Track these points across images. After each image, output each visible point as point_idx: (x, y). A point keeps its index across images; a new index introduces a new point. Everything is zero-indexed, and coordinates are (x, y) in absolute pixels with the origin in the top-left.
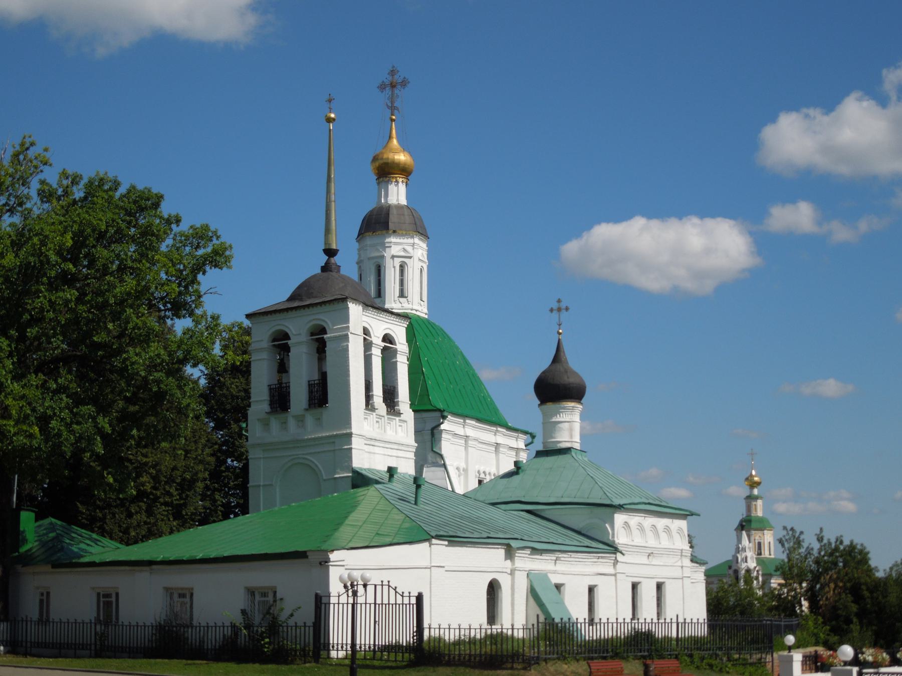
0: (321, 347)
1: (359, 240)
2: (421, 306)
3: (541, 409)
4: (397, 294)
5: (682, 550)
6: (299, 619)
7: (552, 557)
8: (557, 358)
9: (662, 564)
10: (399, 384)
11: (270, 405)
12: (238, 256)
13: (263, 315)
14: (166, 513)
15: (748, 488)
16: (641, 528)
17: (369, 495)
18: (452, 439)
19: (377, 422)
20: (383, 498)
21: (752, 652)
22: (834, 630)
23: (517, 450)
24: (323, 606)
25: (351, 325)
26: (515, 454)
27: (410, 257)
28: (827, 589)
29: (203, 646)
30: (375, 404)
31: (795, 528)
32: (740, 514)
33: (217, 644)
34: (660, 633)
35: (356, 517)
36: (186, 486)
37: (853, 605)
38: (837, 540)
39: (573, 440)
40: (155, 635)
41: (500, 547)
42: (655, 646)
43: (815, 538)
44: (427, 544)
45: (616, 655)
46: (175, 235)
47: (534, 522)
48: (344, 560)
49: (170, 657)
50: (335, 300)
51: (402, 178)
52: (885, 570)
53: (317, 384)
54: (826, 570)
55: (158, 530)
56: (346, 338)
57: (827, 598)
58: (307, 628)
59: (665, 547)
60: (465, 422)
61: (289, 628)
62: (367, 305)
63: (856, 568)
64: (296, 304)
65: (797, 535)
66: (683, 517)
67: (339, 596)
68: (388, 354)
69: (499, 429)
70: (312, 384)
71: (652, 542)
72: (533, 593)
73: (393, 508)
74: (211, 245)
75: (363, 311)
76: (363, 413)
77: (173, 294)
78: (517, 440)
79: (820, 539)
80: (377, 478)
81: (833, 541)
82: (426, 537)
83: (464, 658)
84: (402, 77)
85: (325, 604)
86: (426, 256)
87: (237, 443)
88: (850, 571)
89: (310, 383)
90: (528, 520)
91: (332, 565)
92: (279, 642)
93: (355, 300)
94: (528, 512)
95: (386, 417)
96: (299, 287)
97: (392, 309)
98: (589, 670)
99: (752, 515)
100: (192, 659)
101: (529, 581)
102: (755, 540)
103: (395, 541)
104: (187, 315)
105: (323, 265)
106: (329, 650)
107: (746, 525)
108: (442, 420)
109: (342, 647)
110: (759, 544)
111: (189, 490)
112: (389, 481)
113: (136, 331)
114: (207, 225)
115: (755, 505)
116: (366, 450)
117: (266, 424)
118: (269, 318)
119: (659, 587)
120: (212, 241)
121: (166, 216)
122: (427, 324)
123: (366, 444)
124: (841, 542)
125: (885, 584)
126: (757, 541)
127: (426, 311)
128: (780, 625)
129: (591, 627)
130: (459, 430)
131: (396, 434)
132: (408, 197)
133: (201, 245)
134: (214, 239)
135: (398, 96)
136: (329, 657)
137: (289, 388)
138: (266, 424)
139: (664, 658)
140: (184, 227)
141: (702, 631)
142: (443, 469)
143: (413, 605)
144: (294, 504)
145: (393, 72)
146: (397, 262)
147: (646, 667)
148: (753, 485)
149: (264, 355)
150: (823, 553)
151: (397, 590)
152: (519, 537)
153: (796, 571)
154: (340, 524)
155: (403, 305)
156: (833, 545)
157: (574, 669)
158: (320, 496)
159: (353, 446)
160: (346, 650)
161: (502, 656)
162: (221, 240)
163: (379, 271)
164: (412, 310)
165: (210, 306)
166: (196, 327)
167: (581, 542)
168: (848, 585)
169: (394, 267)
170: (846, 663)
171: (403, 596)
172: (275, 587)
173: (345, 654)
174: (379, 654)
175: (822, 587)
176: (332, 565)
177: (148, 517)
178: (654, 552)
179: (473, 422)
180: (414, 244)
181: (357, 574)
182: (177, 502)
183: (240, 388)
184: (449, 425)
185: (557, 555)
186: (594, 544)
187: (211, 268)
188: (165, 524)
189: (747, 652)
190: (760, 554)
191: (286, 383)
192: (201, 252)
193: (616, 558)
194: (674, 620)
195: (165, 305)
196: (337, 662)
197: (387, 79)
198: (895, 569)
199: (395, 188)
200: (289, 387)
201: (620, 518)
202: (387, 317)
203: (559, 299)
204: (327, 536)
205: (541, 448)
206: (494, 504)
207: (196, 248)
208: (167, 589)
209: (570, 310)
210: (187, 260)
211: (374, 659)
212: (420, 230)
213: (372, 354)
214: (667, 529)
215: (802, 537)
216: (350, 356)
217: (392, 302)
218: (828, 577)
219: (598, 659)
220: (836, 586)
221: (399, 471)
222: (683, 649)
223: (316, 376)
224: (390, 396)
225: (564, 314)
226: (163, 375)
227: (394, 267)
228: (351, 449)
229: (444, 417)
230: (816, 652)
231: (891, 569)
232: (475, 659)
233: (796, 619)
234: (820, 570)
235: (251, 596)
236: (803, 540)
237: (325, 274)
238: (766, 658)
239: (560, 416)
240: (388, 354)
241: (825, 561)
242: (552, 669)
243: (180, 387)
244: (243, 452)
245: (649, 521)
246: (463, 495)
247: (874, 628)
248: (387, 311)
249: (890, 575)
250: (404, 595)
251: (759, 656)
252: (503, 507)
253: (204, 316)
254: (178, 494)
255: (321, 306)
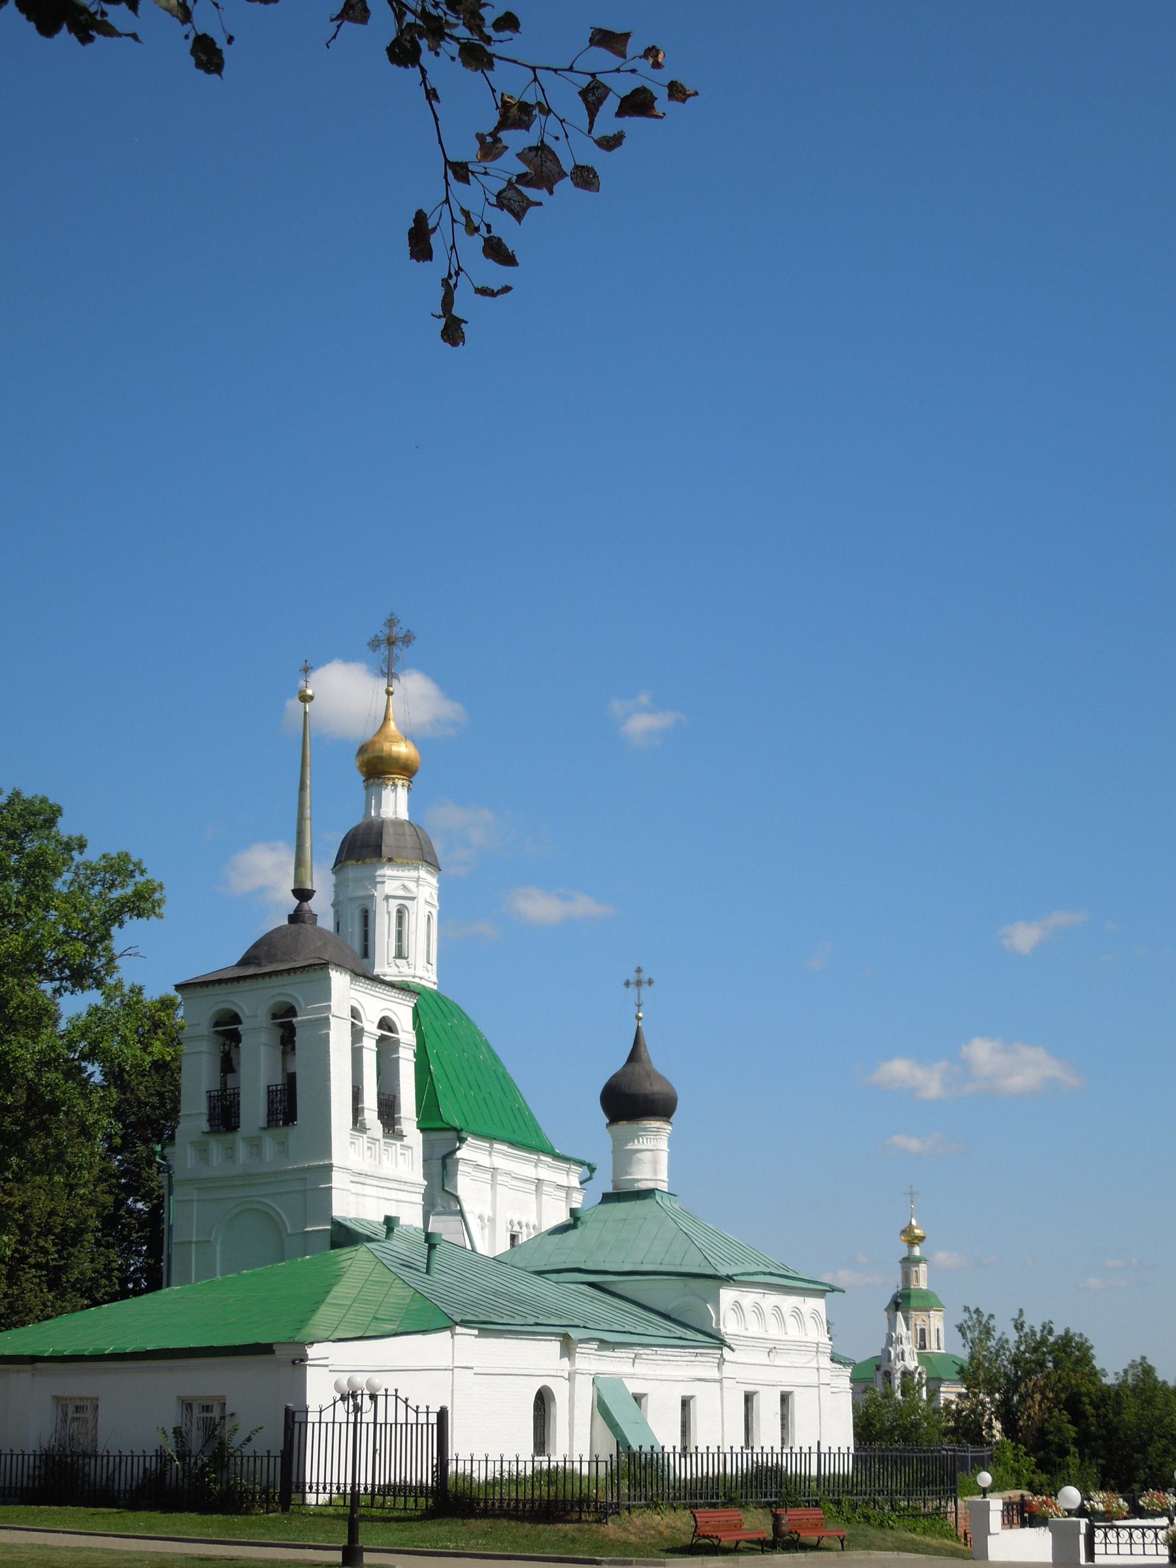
0: (287, 1036)
1: (339, 869)
2: (428, 971)
3: (611, 1132)
4: (393, 953)
5: (817, 1344)
6: (260, 1445)
7: (629, 1353)
8: (635, 1055)
9: (788, 1364)
10: (401, 1091)
11: (209, 1120)
12: (172, 900)
13: (201, 987)
14: (38, 1280)
15: (905, 1245)
16: (758, 1310)
17: (356, 1258)
18: (473, 1173)
19: (369, 1148)
20: (380, 1264)
21: (927, 1497)
22: (1043, 1465)
23: (569, 1189)
24: (297, 1425)
25: (334, 1003)
26: (564, 1195)
27: (413, 899)
28: (1029, 1402)
29: (113, 1486)
30: (367, 1122)
31: (981, 1310)
32: (893, 1285)
33: (135, 1483)
34: (792, 1467)
35: (342, 1292)
36: (69, 1238)
37: (1070, 1426)
38: (1044, 1327)
39: (659, 1178)
40: (40, 1467)
41: (553, 1338)
42: (786, 1488)
43: (1013, 1323)
44: (448, 1333)
45: (730, 1502)
46: (77, 867)
47: (598, 1300)
48: (328, 1358)
49: (60, 1503)
50: (311, 965)
51: (404, 779)
52: (1116, 1374)
53: (280, 1090)
54: (1029, 1373)
55: (24, 1306)
56: (326, 1022)
57: (1029, 1416)
58: (272, 1459)
59: (794, 1339)
60: (491, 1147)
61: (245, 1460)
62: (357, 975)
63: (1073, 1371)
64: (251, 971)
65: (984, 1320)
66: (821, 1294)
67: (321, 1412)
68: (387, 1047)
69: (542, 1158)
70: (273, 1091)
71: (774, 1332)
72: (602, 1408)
73: (395, 1279)
74: (131, 882)
75: (351, 983)
76: (349, 1136)
77: (77, 958)
78: (568, 1175)
79: (1019, 1326)
80: (369, 1233)
81: (1038, 1329)
82: (449, 1325)
83: (508, 1505)
84: (404, 630)
85: (300, 1423)
86: (436, 897)
87: (144, 1175)
88: (1064, 1374)
89: (271, 1088)
90: (592, 1297)
91: (310, 1365)
92: (228, 1481)
93: (339, 966)
94: (592, 1285)
95: (382, 1141)
96: (256, 946)
97: (384, 975)
98: (693, 1523)
99: (912, 1287)
100: (95, 1506)
101: (595, 1390)
102: (915, 1325)
103: (401, 1329)
104: (94, 986)
105: (292, 913)
106: (304, 1493)
107: (901, 1302)
108: (458, 1145)
109: (325, 1488)
110: (923, 1331)
111: (73, 1246)
112: (386, 1238)
113: (21, 1011)
114: (127, 854)
115: (916, 1272)
116: (353, 1191)
117: (203, 1151)
118: (210, 990)
119: (785, 1398)
120: (134, 877)
121: (66, 839)
122: (436, 997)
123: (352, 1182)
124: (1051, 1332)
125: (1117, 1394)
126: (918, 1328)
127: (434, 978)
128: (967, 1457)
129: (683, 1460)
130: (483, 1159)
131: (396, 1166)
132: (411, 808)
133: (116, 883)
134: (137, 874)
135: (398, 658)
136: (304, 1503)
137: (239, 1096)
138: (203, 1151)
139: (799, 1506)
140: (92, 855)
141: (846, 1466)
142: (460, 1218)
143: (433, 1425)
144: (245, 1272)
145: (391, 623)
146: (394, 905)
147: (777, 1518)
148: (913, 1240)
149: (204, 1046)
150: (1022, 1348)
151: (409, 1403)
152: (581, 1324)
153: (982, 1375)
154: (320, 1302)
155: (402, 969)
156: (1038, 1337)
157: (671, 1522)
158: (282, 1260)
159: (334, 1185)
160: (331, 1493)
161: (564, 1501)
162: (147, 876)
163: (366, 918)
164: (414, 977)
165: (128, 973)
166: (107, 1004)
167: (670, 1331)
168: (1063, 1396)
169: (389, 913)
170: (1070, 1512)
171: (417, 1413)
172: (224, 1397)
173: (328, 1499)
174: (379, 1499)
175: (1023, 1398)
176: (310, 1365)
177: (10, 1287)
178: (777, 1347)
179: (504, 1148)
180: (418, 878)
181: (361, 1380)
182: (55, 1263)
183: (152, 1091)
184: (469, 1152)
185: (636, 1351)
186: (690, 1334)
187: (131, 917)
188: (36, 1297)
189: (902, 1497)
190: (923, 1347)
191: (234, 1089)
192: (116, 894)
193: (722, 1355)
194: (814, 1449)
195: (61, 971)
196: (317, 1510)
197: (383, 633)
198: (1130, 1373)
199: (392, 795)
200: (238, 1094)
201: (728, 1295)
202: (385, 992)
203: (639, 967)
204: (302, 1321)
205: (609, 1189)
206: (540, 1273)
207: (109, 889)
208: (57, 1399)
209: (654, 984)
210: (96, 905)
211: (372, 1506)
212: (427, 857)
213: (362, 1047)
214: (797, 1313)
215: (992, 1323)
216: (331, 1050)
217: (385, 966)
218: (1032, 1383)
219: (705, 1507)
220: (1044, 1397)
221: (401, 1222)
222: (826, 1493)
223: (279, 1079)
224: (388, 1109)
225: (645, 988)
226: (61, 1076)
227: (389, 913)
228: (331, 1188)
229: (462, 1140)
230: (1022, 1496)
231: (1126, 1371)
232: (524, 1505)
233: (989, 1448)
234: (1019, 1373)
235: (187, 1409)
236: (994, 1327)
237: (294, 927)
238: (945, 1507)
239: (639, 1142)
240: (387, 1047)
241: (1026, 1359)
242: (638, 1522)
243: (85, 1096)
244: (153, 1188)
245: (771, 1300)
246: (493, 1259)
247: (1101, 1461)
248: (377, 980)
249: (1125, 1381)
250: (419, 1410)
251: (936, 1503)
252: (553, 1276)
253: (118, 986)
254: (56, 1252)
255: (289, 974)
